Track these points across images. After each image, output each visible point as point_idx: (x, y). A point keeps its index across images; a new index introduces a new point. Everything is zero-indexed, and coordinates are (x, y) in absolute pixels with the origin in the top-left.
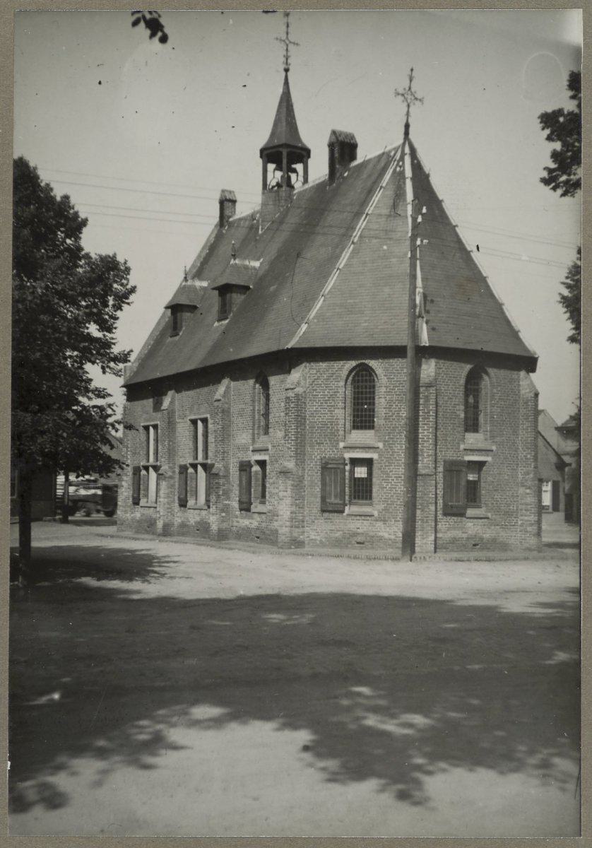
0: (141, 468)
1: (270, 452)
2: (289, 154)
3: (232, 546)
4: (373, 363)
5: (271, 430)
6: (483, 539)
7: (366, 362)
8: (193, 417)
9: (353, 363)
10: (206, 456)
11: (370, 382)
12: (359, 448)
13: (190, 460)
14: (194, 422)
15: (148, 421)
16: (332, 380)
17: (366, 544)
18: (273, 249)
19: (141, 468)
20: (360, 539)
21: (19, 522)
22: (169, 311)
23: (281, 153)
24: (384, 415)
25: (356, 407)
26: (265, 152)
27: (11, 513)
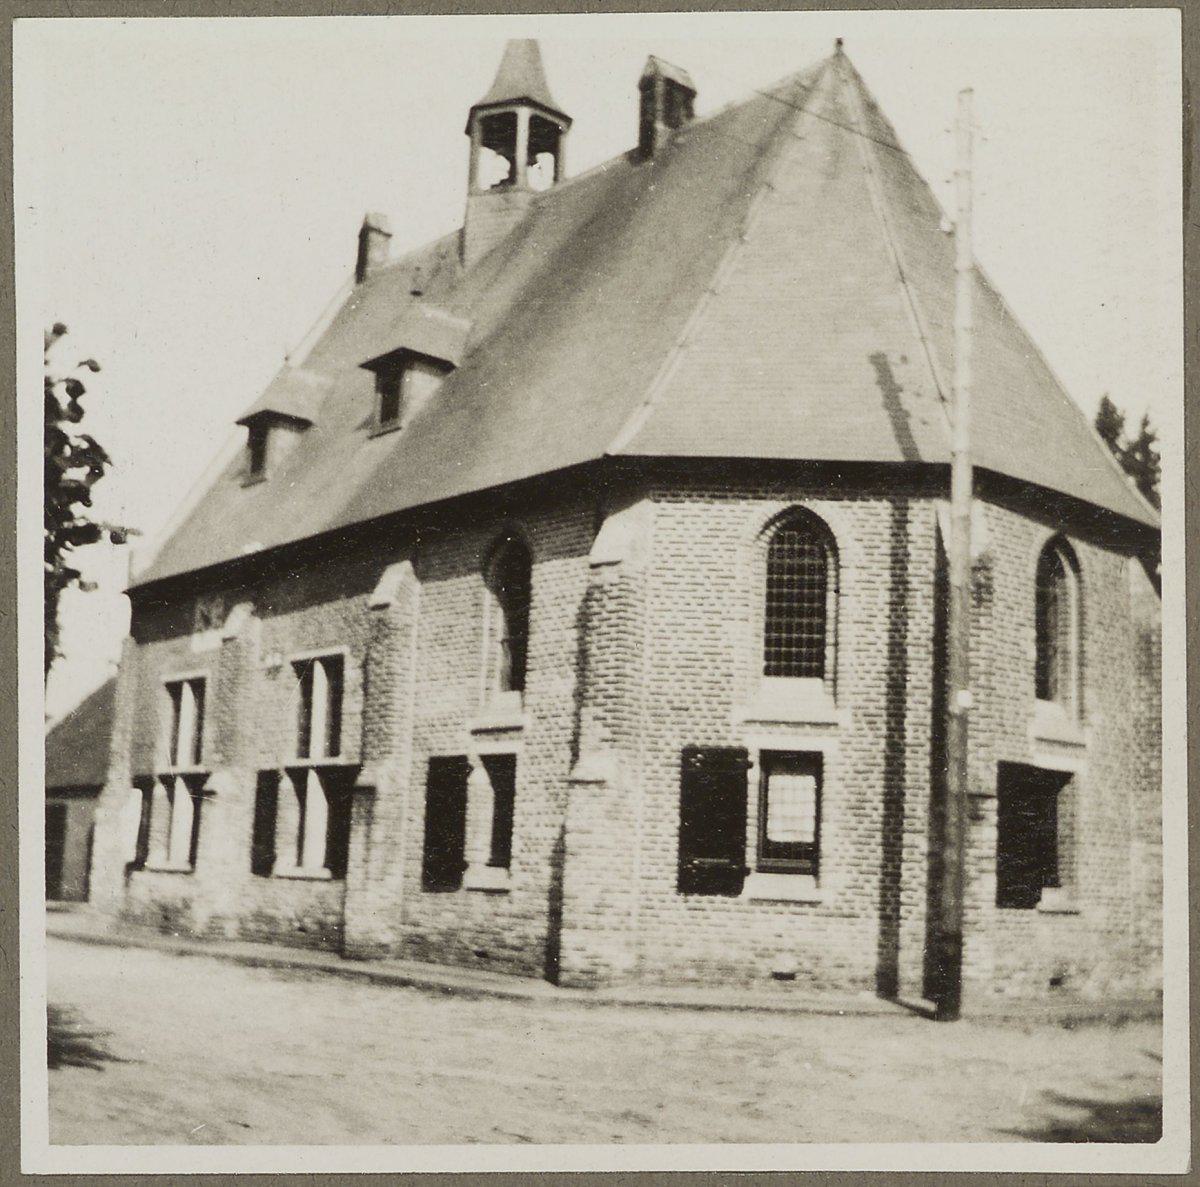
0: (157, 779)
1: (526, 732)
2: (534, 122)
3: (143, 941)
4: (825, 509)
5: (530, 677)
6: (326, 924)
7: (801, 503)
8: (301, 656)
9: (773, 507)
10: (334, 749)
11: (780, 566)
12: (786, 723)
13: (294, 761)
14: (304, 670)
15: (180, 669)
16: (716, 546)
17: (800, 977)
18: (500, 298)
19: (157, 779)
20: (786, 965)
21: (964, 907)
22: (245, 431)
23: (513, 117)
24: (855, 640)
25: (774, 619)
26: (481, 114)
27: (48, 1063)
